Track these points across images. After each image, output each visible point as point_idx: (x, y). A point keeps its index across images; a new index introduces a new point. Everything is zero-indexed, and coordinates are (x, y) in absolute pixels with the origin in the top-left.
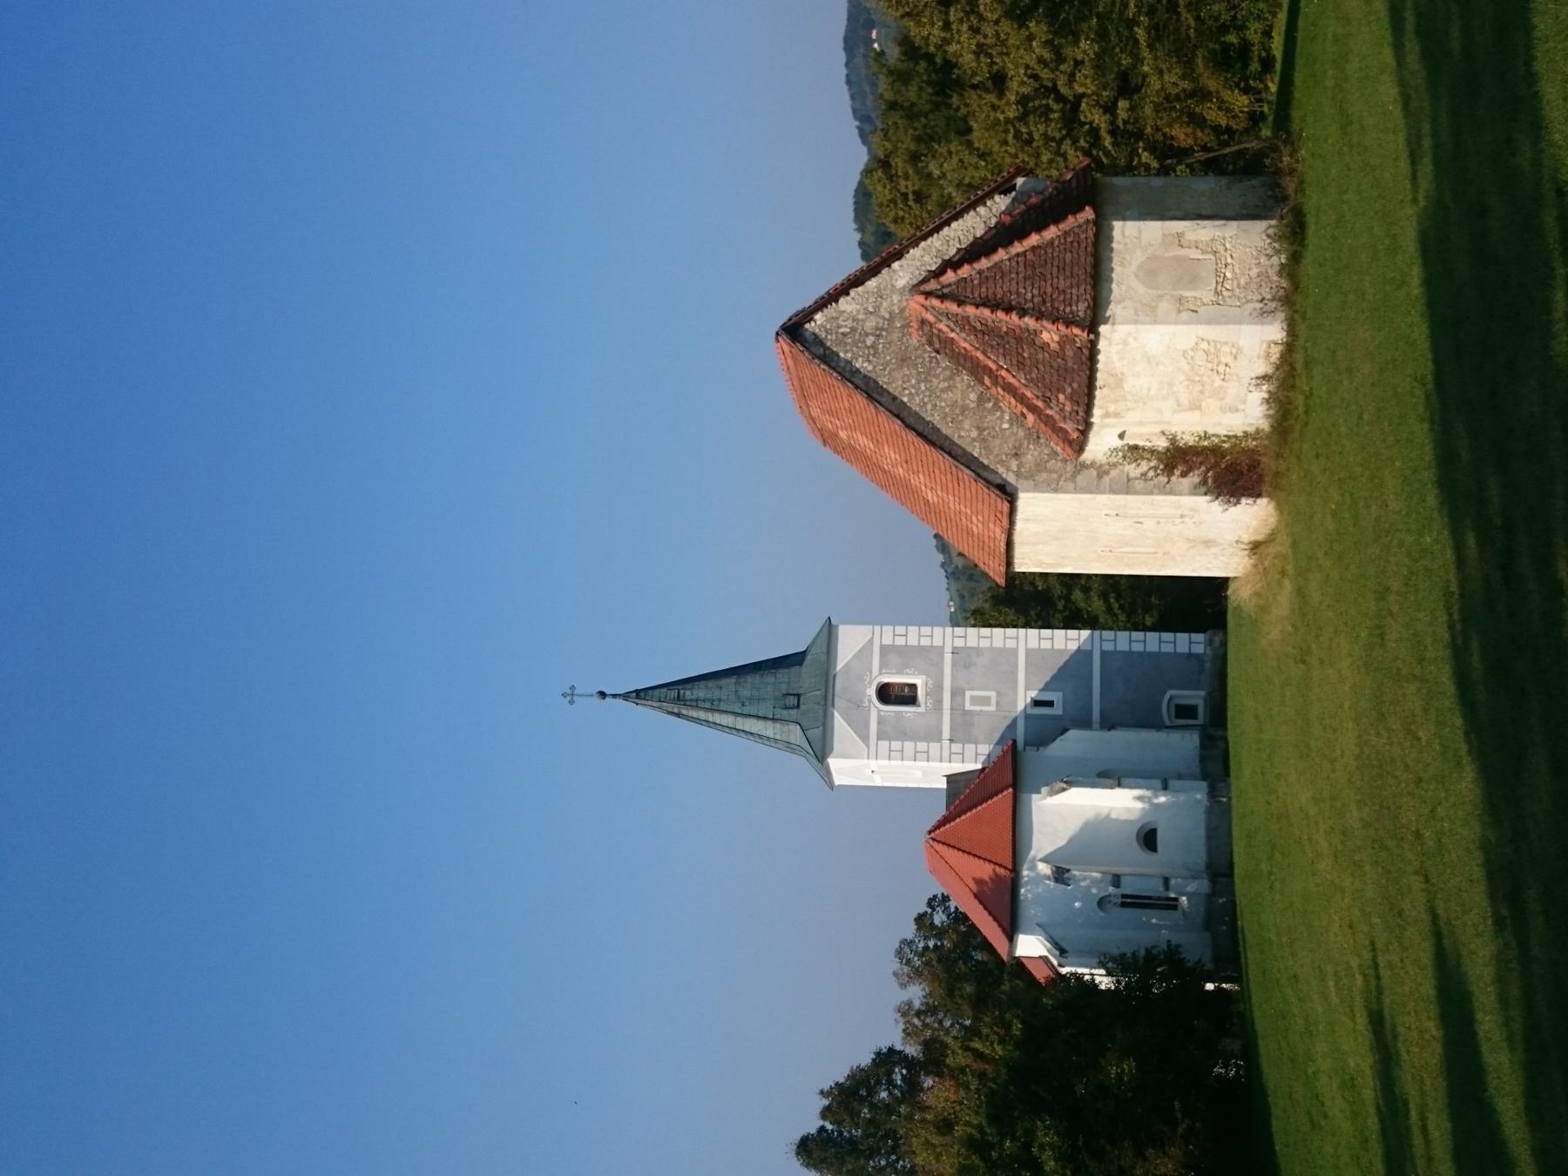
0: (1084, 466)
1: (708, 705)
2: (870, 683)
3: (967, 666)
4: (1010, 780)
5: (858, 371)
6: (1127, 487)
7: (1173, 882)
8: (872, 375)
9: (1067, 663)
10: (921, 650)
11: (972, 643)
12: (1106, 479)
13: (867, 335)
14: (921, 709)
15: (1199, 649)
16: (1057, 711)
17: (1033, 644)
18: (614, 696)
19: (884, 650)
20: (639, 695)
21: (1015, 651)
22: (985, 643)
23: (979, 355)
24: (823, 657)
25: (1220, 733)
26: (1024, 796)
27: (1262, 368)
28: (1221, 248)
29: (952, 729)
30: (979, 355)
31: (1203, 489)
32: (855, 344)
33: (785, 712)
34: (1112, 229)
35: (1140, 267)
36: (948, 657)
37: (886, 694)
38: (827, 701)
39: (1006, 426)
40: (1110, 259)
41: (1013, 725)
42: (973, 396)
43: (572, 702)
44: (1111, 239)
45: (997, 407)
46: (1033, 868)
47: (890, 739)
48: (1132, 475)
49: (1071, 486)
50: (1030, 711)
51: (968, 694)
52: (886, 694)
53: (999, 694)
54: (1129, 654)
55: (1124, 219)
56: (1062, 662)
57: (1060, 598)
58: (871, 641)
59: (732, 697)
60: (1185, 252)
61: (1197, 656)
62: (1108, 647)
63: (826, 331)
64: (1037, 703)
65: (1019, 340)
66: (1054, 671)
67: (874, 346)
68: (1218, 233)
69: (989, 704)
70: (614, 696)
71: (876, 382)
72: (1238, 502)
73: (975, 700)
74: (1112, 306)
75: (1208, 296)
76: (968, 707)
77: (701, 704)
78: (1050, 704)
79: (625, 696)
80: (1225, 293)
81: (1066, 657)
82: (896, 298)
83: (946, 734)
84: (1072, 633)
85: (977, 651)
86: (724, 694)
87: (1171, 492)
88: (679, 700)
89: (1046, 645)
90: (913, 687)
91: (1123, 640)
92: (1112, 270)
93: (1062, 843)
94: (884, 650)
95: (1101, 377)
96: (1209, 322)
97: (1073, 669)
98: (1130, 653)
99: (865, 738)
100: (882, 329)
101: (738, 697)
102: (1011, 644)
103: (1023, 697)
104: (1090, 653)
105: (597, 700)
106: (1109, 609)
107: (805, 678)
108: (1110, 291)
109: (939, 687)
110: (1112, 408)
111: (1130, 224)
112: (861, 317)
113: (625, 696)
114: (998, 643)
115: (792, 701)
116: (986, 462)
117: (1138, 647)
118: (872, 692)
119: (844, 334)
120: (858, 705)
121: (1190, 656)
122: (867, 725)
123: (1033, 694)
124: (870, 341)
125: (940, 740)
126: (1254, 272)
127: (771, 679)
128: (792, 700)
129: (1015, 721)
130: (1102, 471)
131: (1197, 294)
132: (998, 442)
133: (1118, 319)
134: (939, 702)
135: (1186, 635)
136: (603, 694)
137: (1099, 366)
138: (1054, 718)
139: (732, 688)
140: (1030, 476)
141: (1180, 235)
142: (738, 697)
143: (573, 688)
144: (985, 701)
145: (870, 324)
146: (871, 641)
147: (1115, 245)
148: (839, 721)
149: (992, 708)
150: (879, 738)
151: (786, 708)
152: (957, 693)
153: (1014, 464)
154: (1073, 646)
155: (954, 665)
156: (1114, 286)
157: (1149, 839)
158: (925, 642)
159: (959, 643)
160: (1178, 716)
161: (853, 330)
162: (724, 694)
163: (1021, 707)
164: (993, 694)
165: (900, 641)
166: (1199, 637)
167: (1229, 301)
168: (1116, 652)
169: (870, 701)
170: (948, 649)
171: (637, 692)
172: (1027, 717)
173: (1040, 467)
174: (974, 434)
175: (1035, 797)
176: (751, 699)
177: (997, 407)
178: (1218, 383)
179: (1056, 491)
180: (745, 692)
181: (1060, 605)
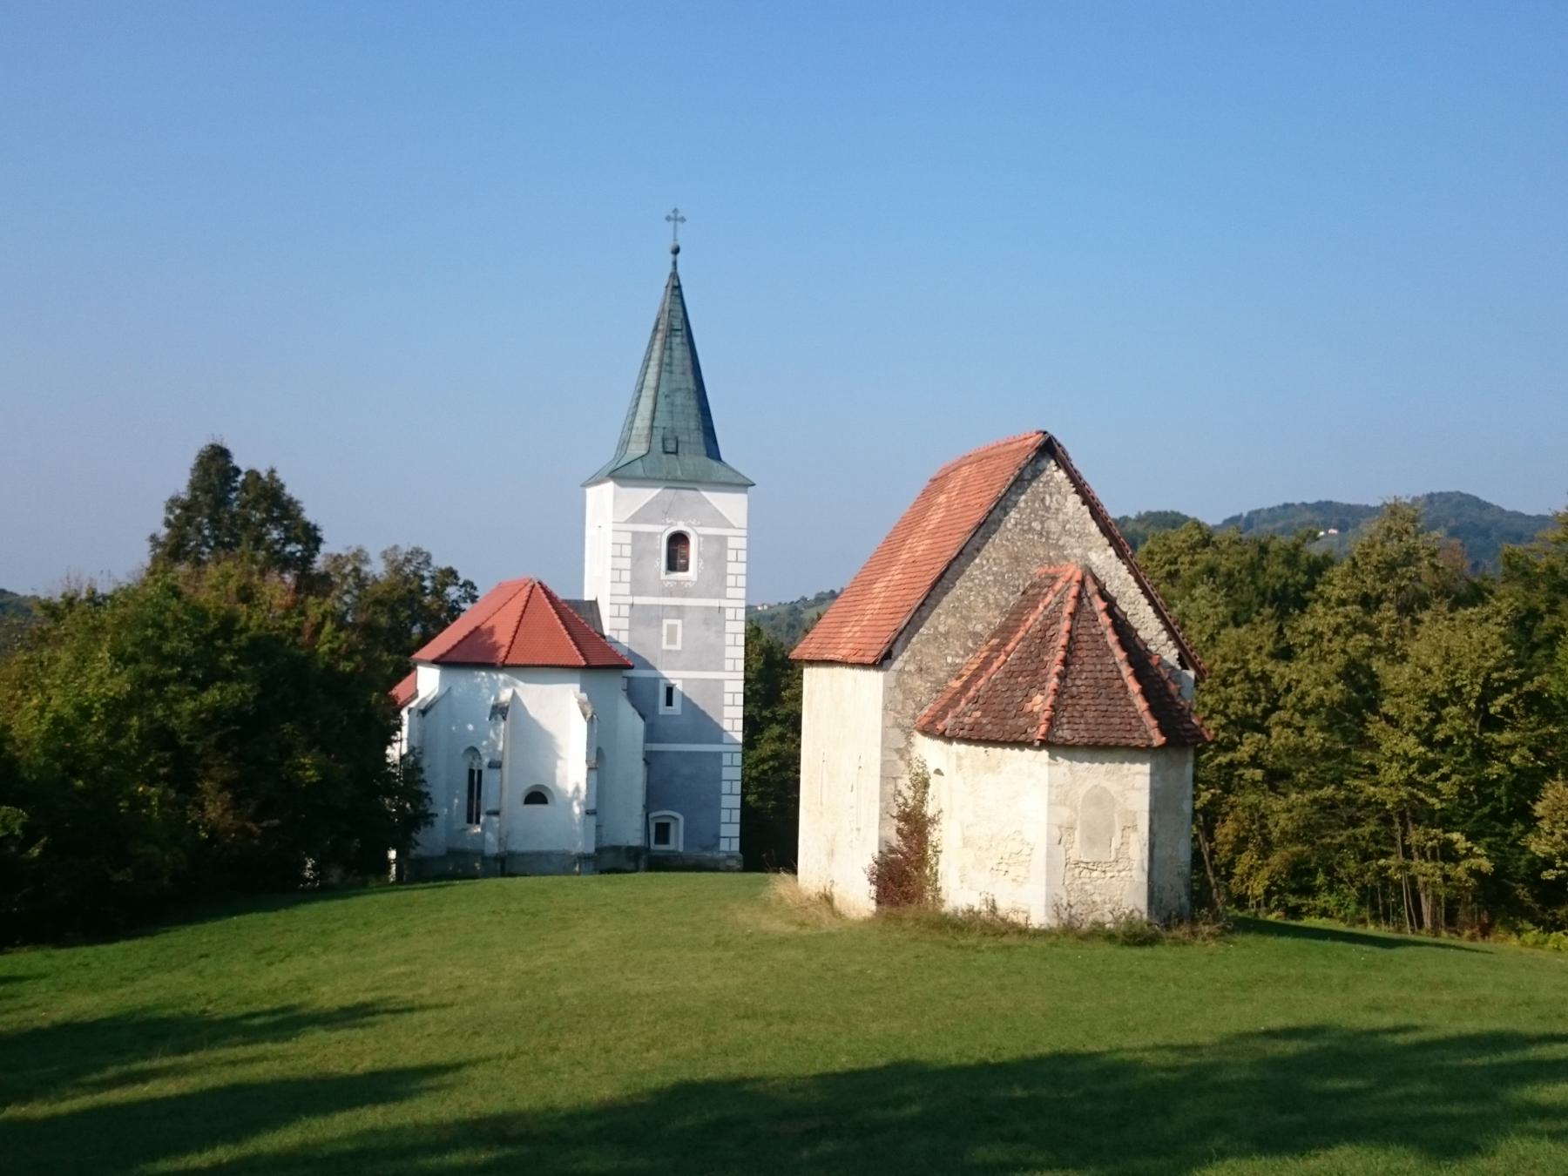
0: (909, 735)
2: (690, 525)
3: (706, 622)
4: (594, 662)
5: (1006, 514)
6: (888, 777)
7: (495, 819)
9: (710, 719)
10: (722, 576)
11: (730, 627)
12: (896, 757)
13: (1042, 523)
14: (663, 576)
15: (724, 846)
16: (663, 709)
17: (728, 686)
18: (675, 263)
19: (722, 540)
20: (676, 289)
21: (721, 668)
22: (729, 639)
23: (1021, 634)
25: (642, 865)
26: (577, 676)
27: (1004, 907)
28: (1121, 867)
29: (644, 606)
30: (1021, 634)
31: (885, 850)
33: (659, 439)
34: (1143, 762)
35: (1104, 790)
36: (715, 603)
37: (678, 541)
39: (949, 659)
41: (647, 666)
42: (979, 628)
43: (668, 219)
44: (1132, 761)
45: (968, 651)
46: (506, 684)
47: (633, 544)
48: (900, 782)
49: (890, 722)
50: (662, 683)
51: (679, 622)
52: (678, 541)
53: (678, 653)
54: (718, 779)
56: (710, 714)
59: (674, 385)
60: (1118, 833)
61: (717, 844)
62: (726, 759)
64: (670, 690)
65: (1035, 673)
67: (1031, 529)
69: (668, 642)
70: (675, 263)
72: (872, 883)
73: (672, 629)
74: (1067, 763)
76: (666, 622)
78: (669, 702)
79: (674, 275)
81: (716, 719)
82: (1078, 551)
83: (638, 600)
84: (739, 725)
85: (721, 632)
87: (882, 819)
88: (672, 331)
89: (728, 699)
90: (685, 568)
91: (732, 774)
92: (1102, 763)
93: (532, 712)
94: (722, 540)
95: (996, 752)
96: (1049, 855)
97: (707, 728)
99: (634, 519)
102: (729, 664)
103: (676, 677)
104: (719, 741)
106: (763, 761)
107: (694, 460)
110: (966, 762)
112: (1061, 517)
113: (674, 275)
114: (729, 652)
115: (671, 446)
116: (914, 640)
117: (725, 787)
118: (680, 527)
119: (1043, 500)
121: (718, 837)
123: (679, 686)
124: (1037, 525)
125: (633, 594)
130: (903, 753)
132: (934, 651)
134: (671, 595)
136: (676, 251)
137: (1008, 750)
138: (655, 707)
140: (900, 684)
141: (1134, 828)
144: (672, 640)
145: (1053, 526)
147: (1126, 765)
148: (648, 494)
149: (665, 646)
150: (634, 534)
151: (664, 440)
152: (679, 611)
153: (911, 667)
154: (726, 725)
155: (707, 608)
156: (1086, 764)
158: (730, 580)
159: (729, 614)
161: (1047, 509)
162: (678, 376)
163: (666, 674)
164: (678, 647)
165: (731, 555)
166: (736, 846)
169: (671, 525)
170: (724, 603)
171: (679, 287)
172: (656, 680)
173: (908, 693)
174: (942, 629)
175: (577, 687)
176: (672, 404)
177: (968, 651)
178: (990, 864)
179: (885, 708)
180: (679, 399)
181: (766, 713)
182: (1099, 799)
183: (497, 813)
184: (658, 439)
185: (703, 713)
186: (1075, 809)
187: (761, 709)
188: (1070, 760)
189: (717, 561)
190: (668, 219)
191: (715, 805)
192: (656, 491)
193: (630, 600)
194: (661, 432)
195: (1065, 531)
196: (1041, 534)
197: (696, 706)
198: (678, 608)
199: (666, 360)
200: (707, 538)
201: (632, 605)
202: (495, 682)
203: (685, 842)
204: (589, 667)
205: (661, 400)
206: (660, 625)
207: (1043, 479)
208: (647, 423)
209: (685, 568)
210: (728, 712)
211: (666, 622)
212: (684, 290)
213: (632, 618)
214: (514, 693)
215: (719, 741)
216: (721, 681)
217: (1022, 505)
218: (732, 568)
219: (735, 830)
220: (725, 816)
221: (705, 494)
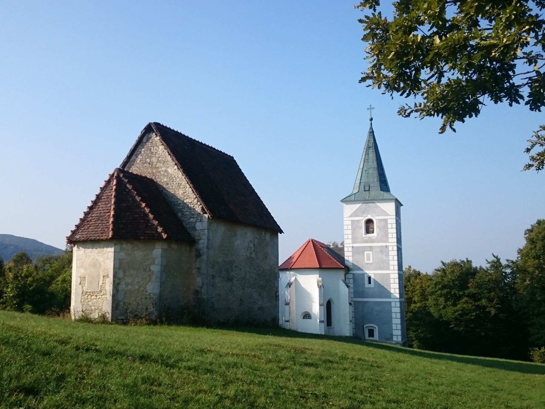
1: (366, 158)
2: (372, 216)
3: (381, 251)
5: (137, 157)
7: (288, 323)
8: (135, 163)
9: (386, 289)
10: (386, 234)
11: (391, 253)
14: (364, 236)
15: (395, 339)
16: (367, 285)
17: (392, 276)
19: (386, 220)
20: (372, 132)
21: (389, 269)
22: (391, 258)
24: (381, 198)
26: (318, 271)
28: (102, 294)
29: (357, 247)
32: (147, 155)
33: (363, 186)
34: (111, 247)
35: (97, 260)
36: (384, 244)
37: (369, 222)
38: (365, 201)
40: (100, 248)
41: (359, 269)
43: (368, 109)
44: (107, 247)
46: (294, 275)
47: (352, 225)
50: (366, 275)
51: (371, 252)
52: (369, 222)
53: (372, 264)
54: (391, 312)
55: (115, 252)
56: (386, 287)
57: (464, 293)
58: (390, 215)
59: (369, 167)
61: (392, 338)
62: (393, 304)
63: (152, 142)
64: (370, 278)
66: (382, 284)
67: (146, 162)
68: (108, 292)
69: (367, 260)
71: (133, 165)
73: (368, 255)
74: (83, 249)
75: (85, 289)
76: (366, 253)
77: (367, 156)
78: (370, 283)
79: (371, 128)
80: (86, 296)
81: (388, 289)
82: (164, 169)
83: (355, 245)
84: (397, 291)
85: (388, 255)
86: (370, 163)
88: (368, 148)
89: (392, 281)
90: (373, 232)
91: (396, 310)
92: (96, 249)
93: (303, 285)
94: (386, 220)
97: (384, 292)
98: (391, 313)
99: (351, 216)
100: (152, 165)
101: (369, 169)
102: (391, 268)
103: (371, 273)
104: (390, 297)
105: (369, 118)
106: (457, 311)
107: (376, 191)
108: (89, 249)
109: (372, 241)
111: (113, 254)
112: (157, 155)
113: (371, 128)
114: (391, 263)
115: (367, 188)
117: (394, 315)
118: (369, 217)
119: (150, 149)
120: (364, 212)
121: (392, 335)
122: (356, 216)
123: (372, 277)
124: (148, 160)
125: (353, 243)
126: (93, 308)
127: (375, 180)
128: (367, 189)
129: (363, 270)
131: (86, 285)
133: (79, 252)
134: (367, 242)
135: (400, 334)
136: (371, 120)
138: (364, 284)
139: (373, 166)
141: (108, 276)
142: (369, 169)
143: (373, 108)
144: (368, 259)
145: (154, 160)
146: (390, 215)
147: (105, 249)
148: (356, 206)
149: (366, 262)
150: (352, 221)
151: (364, 186)
152: (371, 248)
154: (392, 291)
155: (381, 246)
156: (91, 249)
157: (307, 316)
158: (390, 235)
159: (390, 248)
160: (369, 330)
161: (152, 153)
162: (370, 163)
163: (367, 272)
164: (371, 261)
165: (390, 226)
166: (400, 339)
167: (83, 297)
168: (391, 307)
169: (366, 216)
170: (388, 244)
171: (373, 132)
172: (363, 274)
175: (318, 276)
176: (368, 173)
180: (371, 171)
181: (461, 293)
182: (95, 265)
183: (288, 321)
184: (362, 187)
185: (383, 287)
186: (86, 269)
187: (459, 291)
188: (84, 248)
189: (385, 229)
190: (368, 109)
191: (390, 323)
192: (360, 205)
193: (351, 245)
194: (363, 184)
195: (159, 161)
196: (149, 163)
197: (380, 284)
198: (370, 247)
199: (366, 158)
200: (380, 220)
201: (353, 247)
202: (291, 275)
203: (379, 337)
204: (320, 268)
205: (364, 172)
206: (364, 254)
207: (150, 141)
208: (359, 181)
209: (373, 232)
210: (392, 286)
211: (366, 253)
212: (375, 133)
213: (353, 252)
214: (296, 278)
215: (390, 297)
216: (389, 274)
217: (143, 153)
218: (390, 231)
219: (399, 333)
220: (394, 327)
221: (379, 204)
